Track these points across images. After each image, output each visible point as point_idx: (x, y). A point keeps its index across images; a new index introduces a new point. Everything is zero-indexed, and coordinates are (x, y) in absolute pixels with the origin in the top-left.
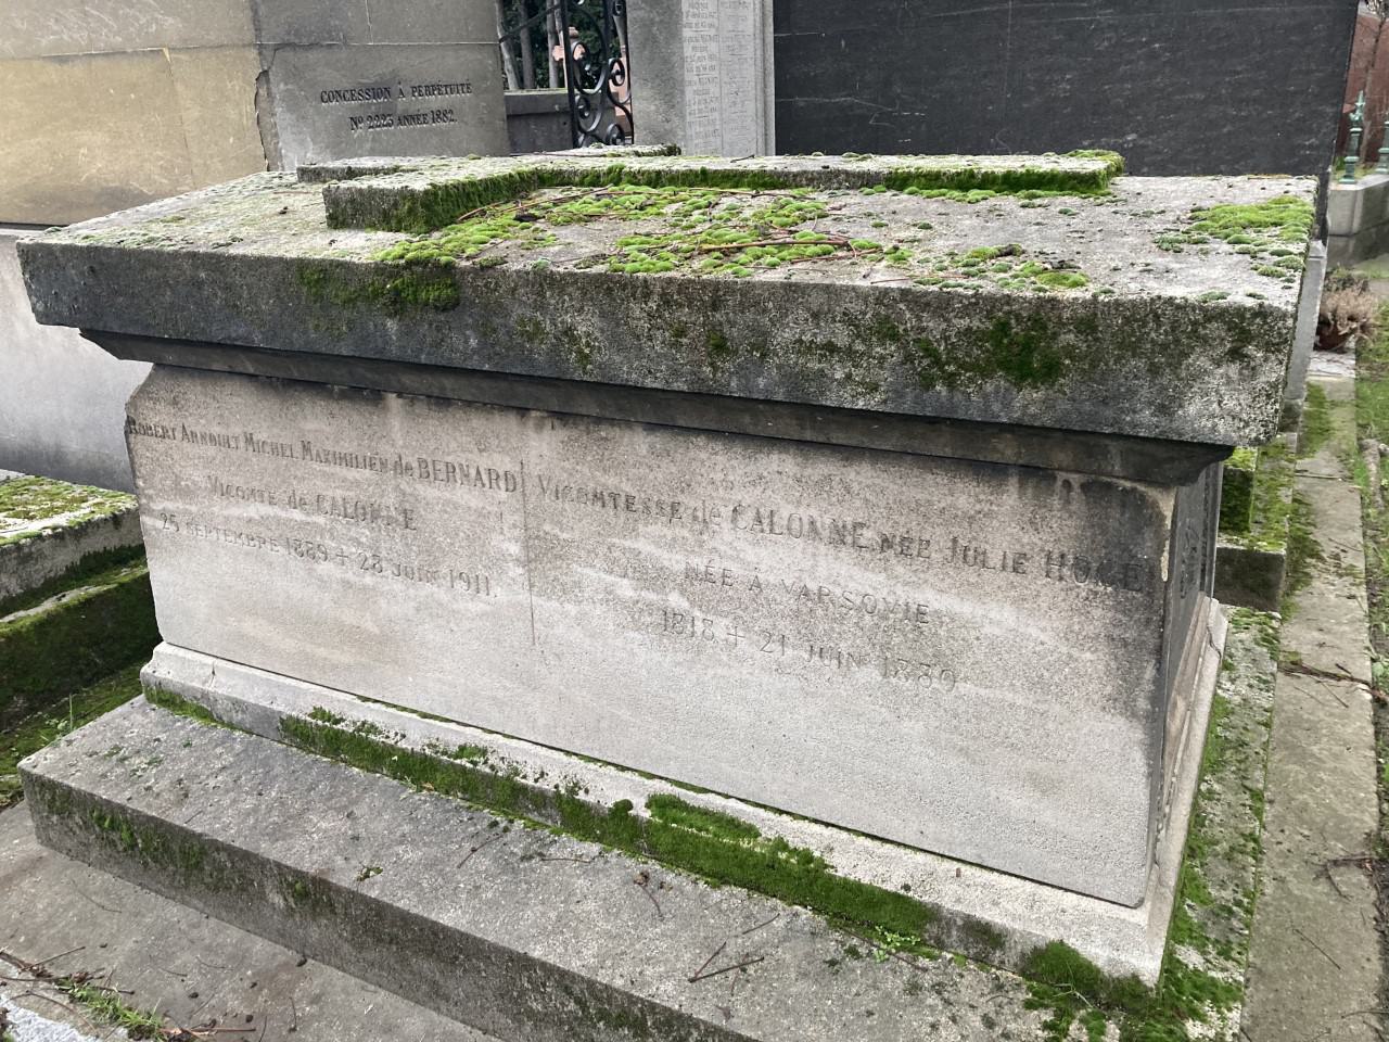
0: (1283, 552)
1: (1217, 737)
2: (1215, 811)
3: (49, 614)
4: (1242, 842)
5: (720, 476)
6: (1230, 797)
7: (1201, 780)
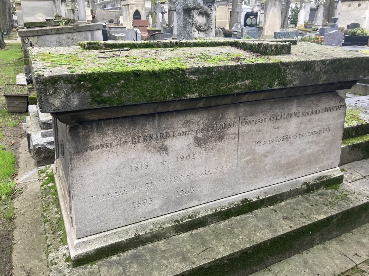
0: (177, 224)
1: (61, 230)
2: (55, 210)
3: (238, 65)
4: (47, 208)
5: (235, 178)
6: (53, 216)
7: (61, 215)
